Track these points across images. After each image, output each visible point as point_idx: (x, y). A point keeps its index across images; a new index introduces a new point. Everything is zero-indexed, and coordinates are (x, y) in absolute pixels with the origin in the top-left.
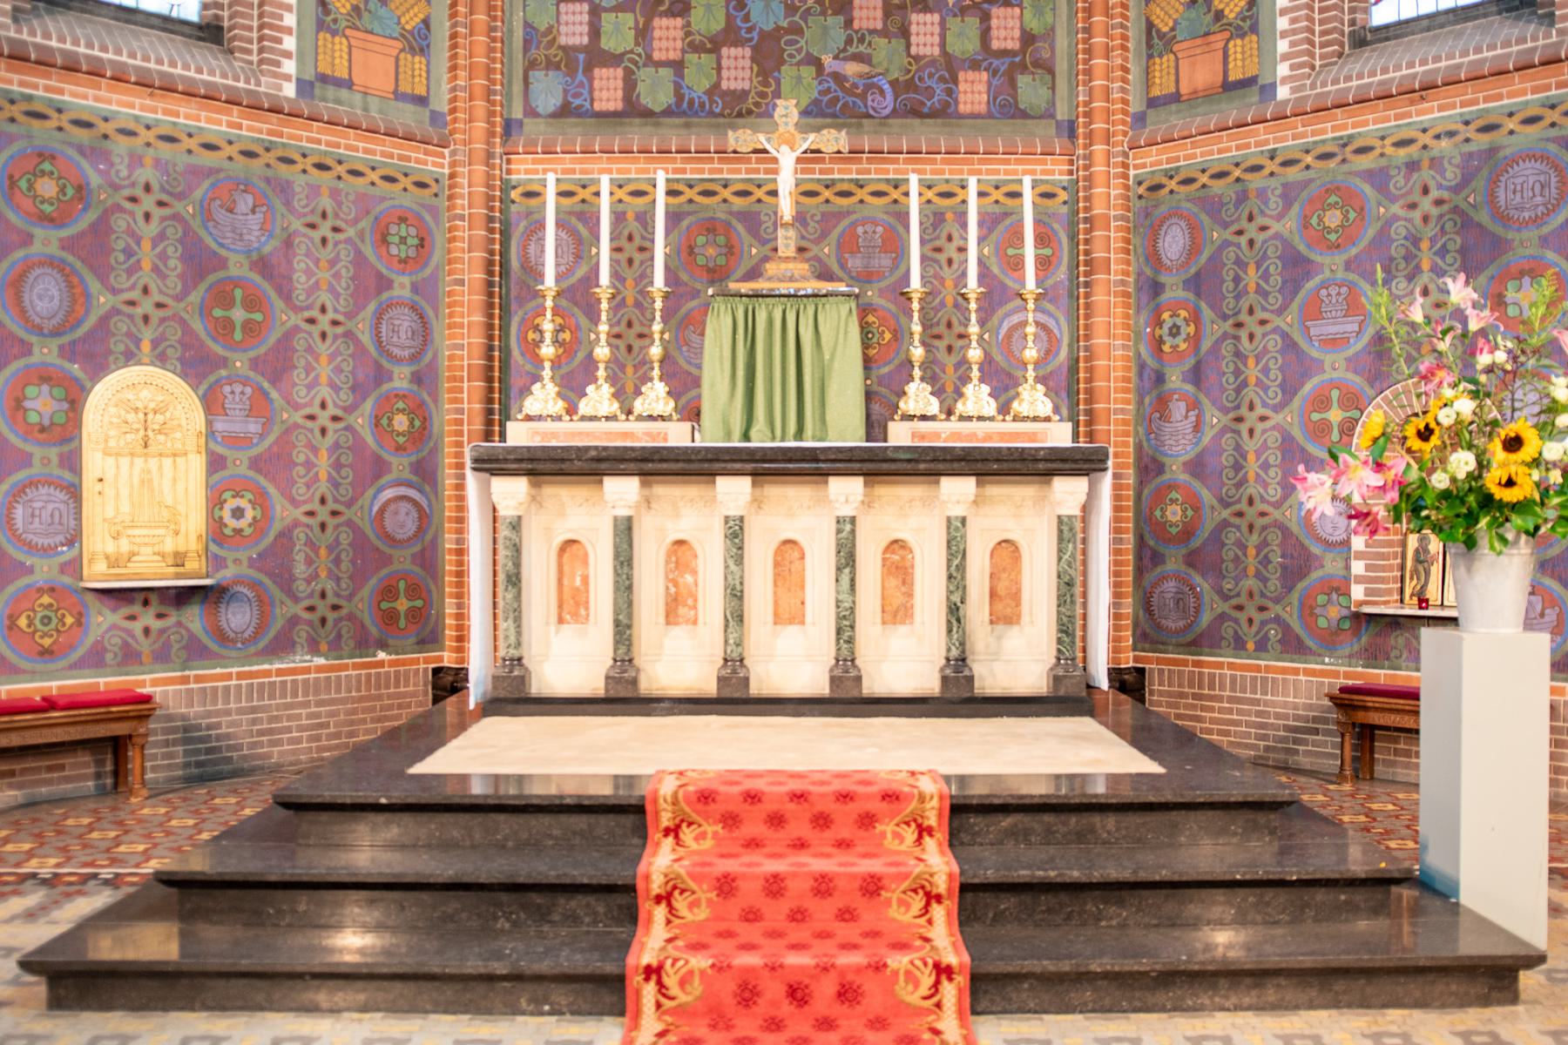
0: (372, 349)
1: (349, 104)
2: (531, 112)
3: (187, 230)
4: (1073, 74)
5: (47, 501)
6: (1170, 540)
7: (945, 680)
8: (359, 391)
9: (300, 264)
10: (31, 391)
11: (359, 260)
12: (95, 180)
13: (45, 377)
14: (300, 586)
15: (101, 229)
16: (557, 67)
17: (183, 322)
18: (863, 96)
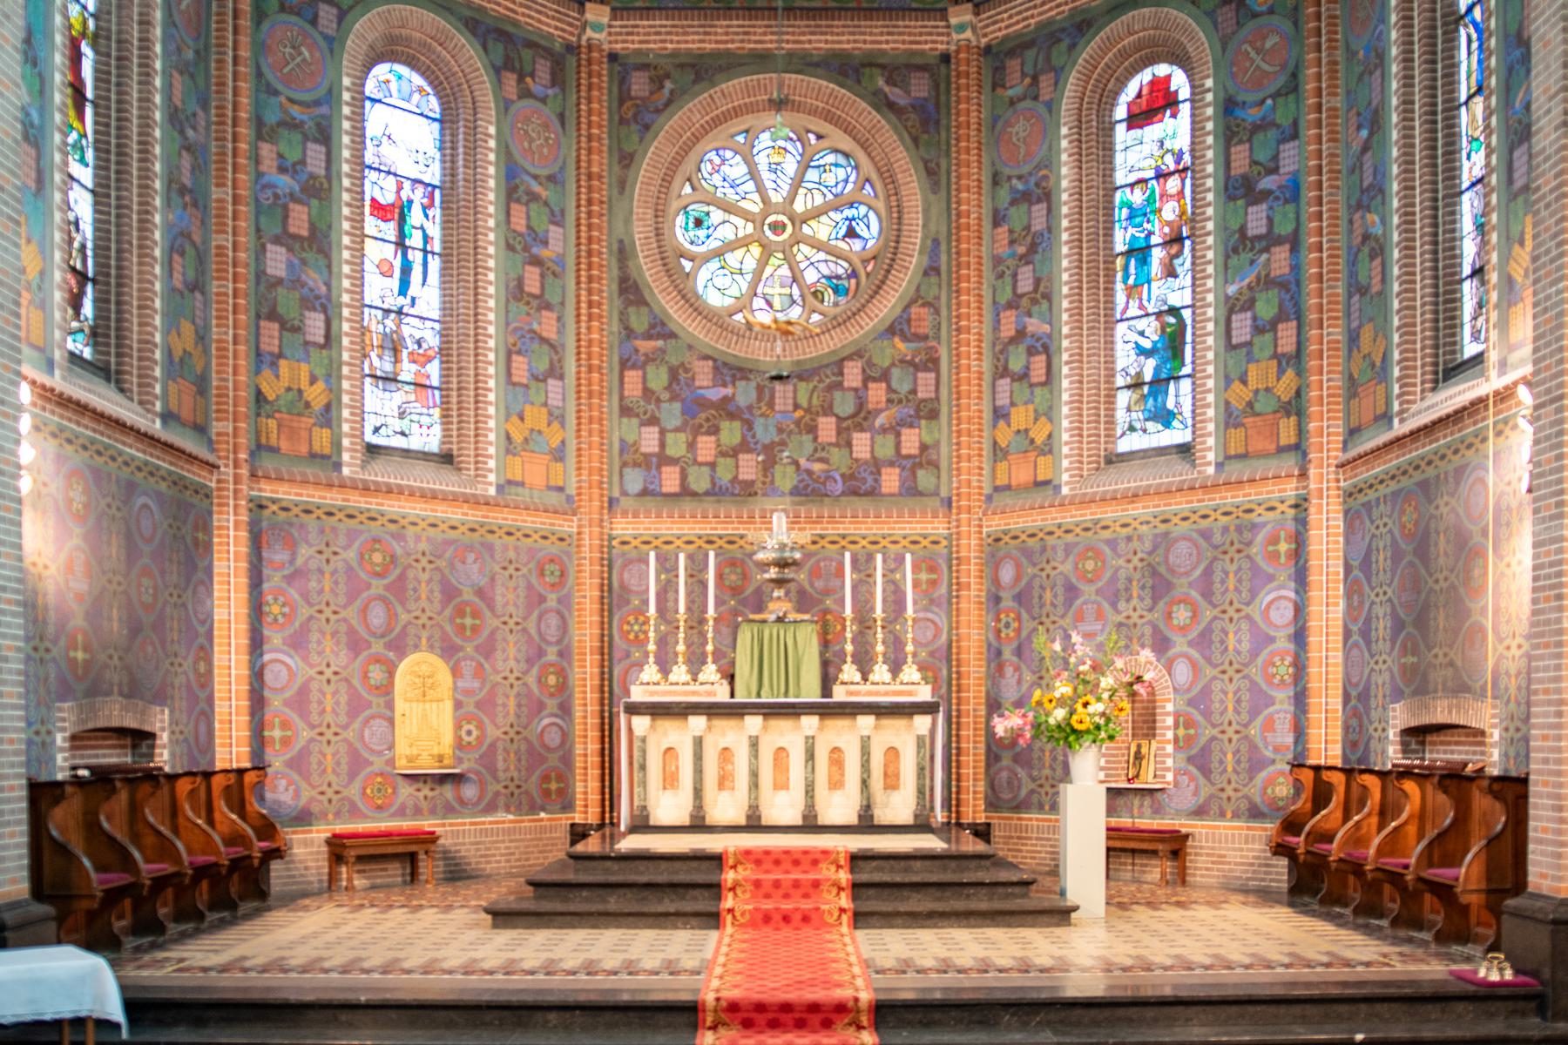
0: (537, 638)
1: (523, 495)
2: (624, 493)
3: (443, 575)
4: (950, 469)
5: (379, 726)
6: (1005, 747)
7: (860, 816)
8: (530, 662)
9: (499, 590)
10: (371, 668)
11: (530, 587)
12: (399, 551)
13: (377, 660)
14: (501, 775)
15: (402, 578)
16: (639, 465)
17: (441, 627)
18: (824, 484)
